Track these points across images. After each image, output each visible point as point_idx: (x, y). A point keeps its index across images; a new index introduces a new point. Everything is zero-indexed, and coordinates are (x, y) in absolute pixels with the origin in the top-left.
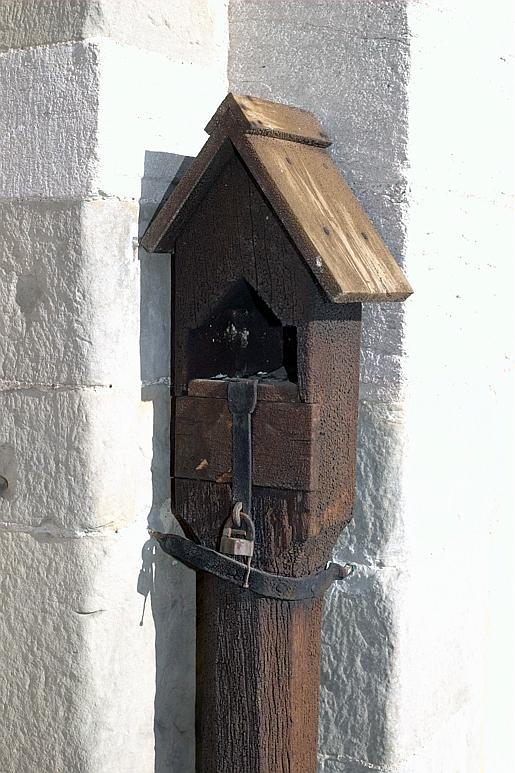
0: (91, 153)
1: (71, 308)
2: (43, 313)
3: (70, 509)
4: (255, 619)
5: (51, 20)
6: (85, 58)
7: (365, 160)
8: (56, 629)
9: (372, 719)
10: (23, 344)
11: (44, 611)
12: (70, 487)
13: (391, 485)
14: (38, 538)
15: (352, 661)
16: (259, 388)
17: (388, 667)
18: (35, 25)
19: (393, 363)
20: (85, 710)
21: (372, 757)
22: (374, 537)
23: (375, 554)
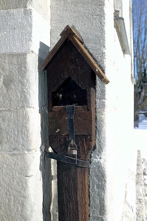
0: (30, 40)
1: (23, 85)
2: (13, 87)
3: (23, 145)
4: (76, 174)
5: (16, 2)
6: (28, 13)
7: (93, 47)
8: (18, 183)
9: (100, 203)
10: (6, 96)
11: (13, 178)
12: (23, 138)
13: (103, 135)
14: (11, 155)
15: (93, 187)
16: (76, 107)
17: (104, 187)
18: (10, 3)
19: (103, 102)
20: (28, 207)
21: (101, 213)
22: (99, 150)
23: (99, 155)
